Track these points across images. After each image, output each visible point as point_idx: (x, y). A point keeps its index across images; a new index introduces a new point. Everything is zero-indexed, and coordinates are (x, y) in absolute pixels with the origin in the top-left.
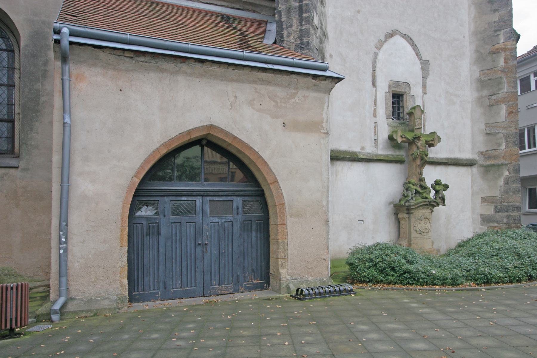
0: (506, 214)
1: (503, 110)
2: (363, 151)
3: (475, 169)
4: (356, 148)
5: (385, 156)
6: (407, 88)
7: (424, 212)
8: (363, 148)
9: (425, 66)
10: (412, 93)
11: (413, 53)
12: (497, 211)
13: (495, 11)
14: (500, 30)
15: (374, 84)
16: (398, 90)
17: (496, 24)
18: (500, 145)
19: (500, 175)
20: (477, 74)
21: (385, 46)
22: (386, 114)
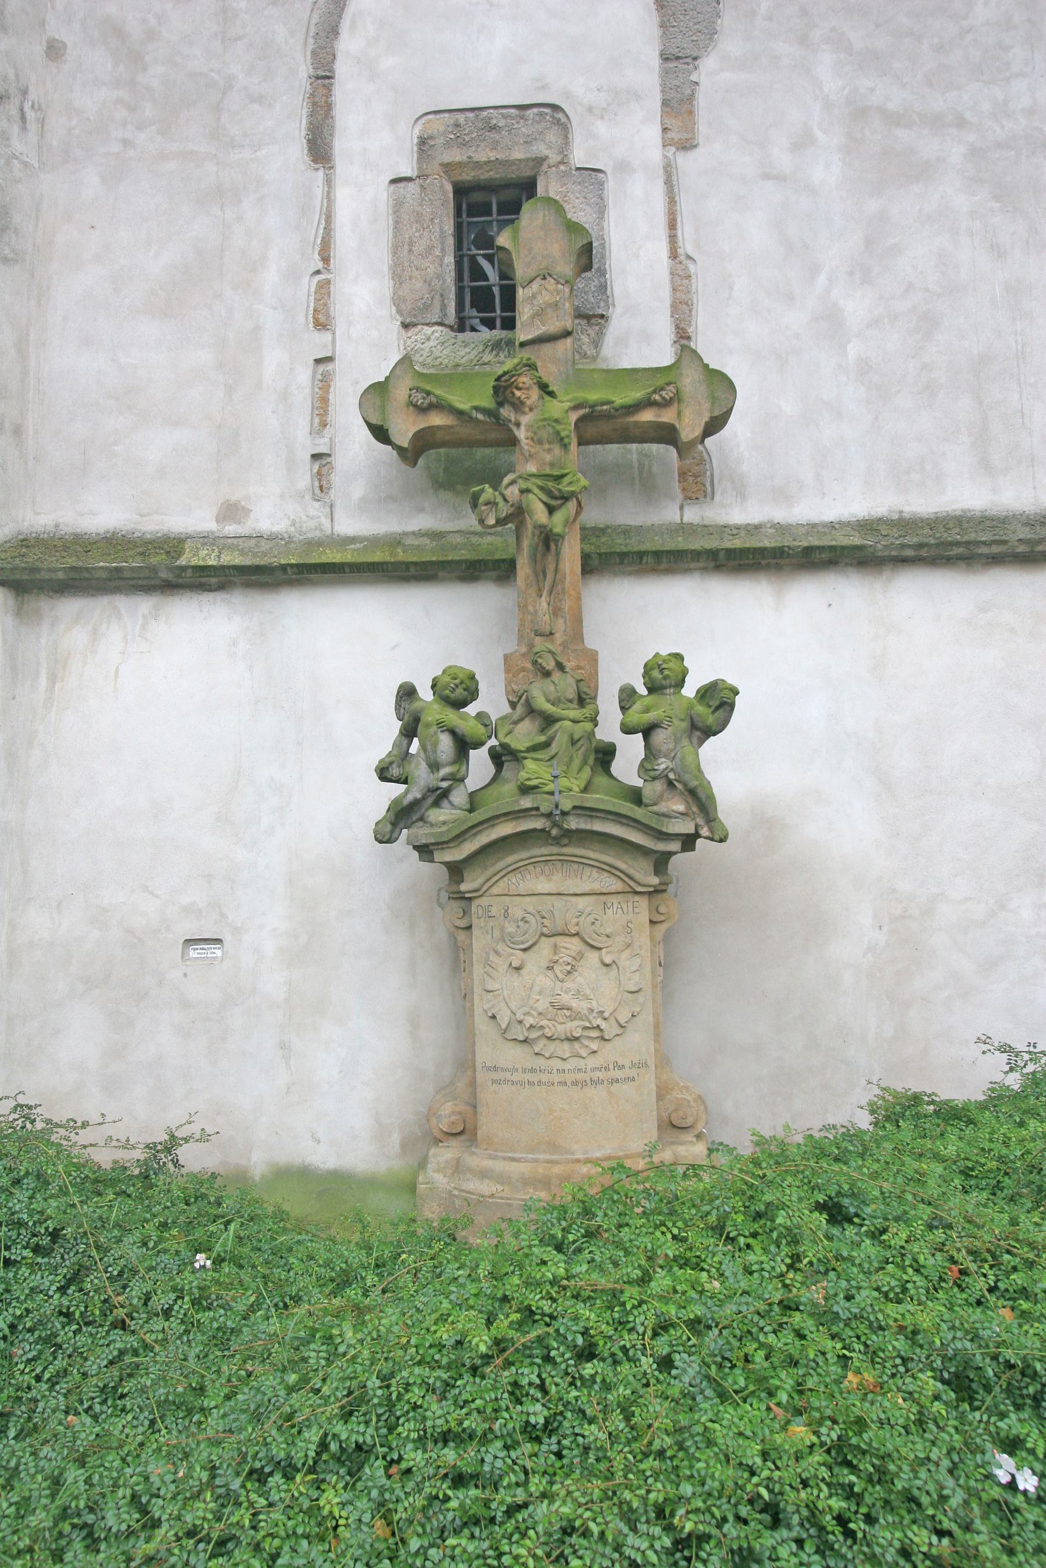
2: (231, 529)
4: (186, 514)
5: (374, 542)
6: (553, 136)
7: (543, 885)
8: (231, 511)
10: (579, 157)
15: (319, 150)
16: (483, 155)
22: (398, 301)
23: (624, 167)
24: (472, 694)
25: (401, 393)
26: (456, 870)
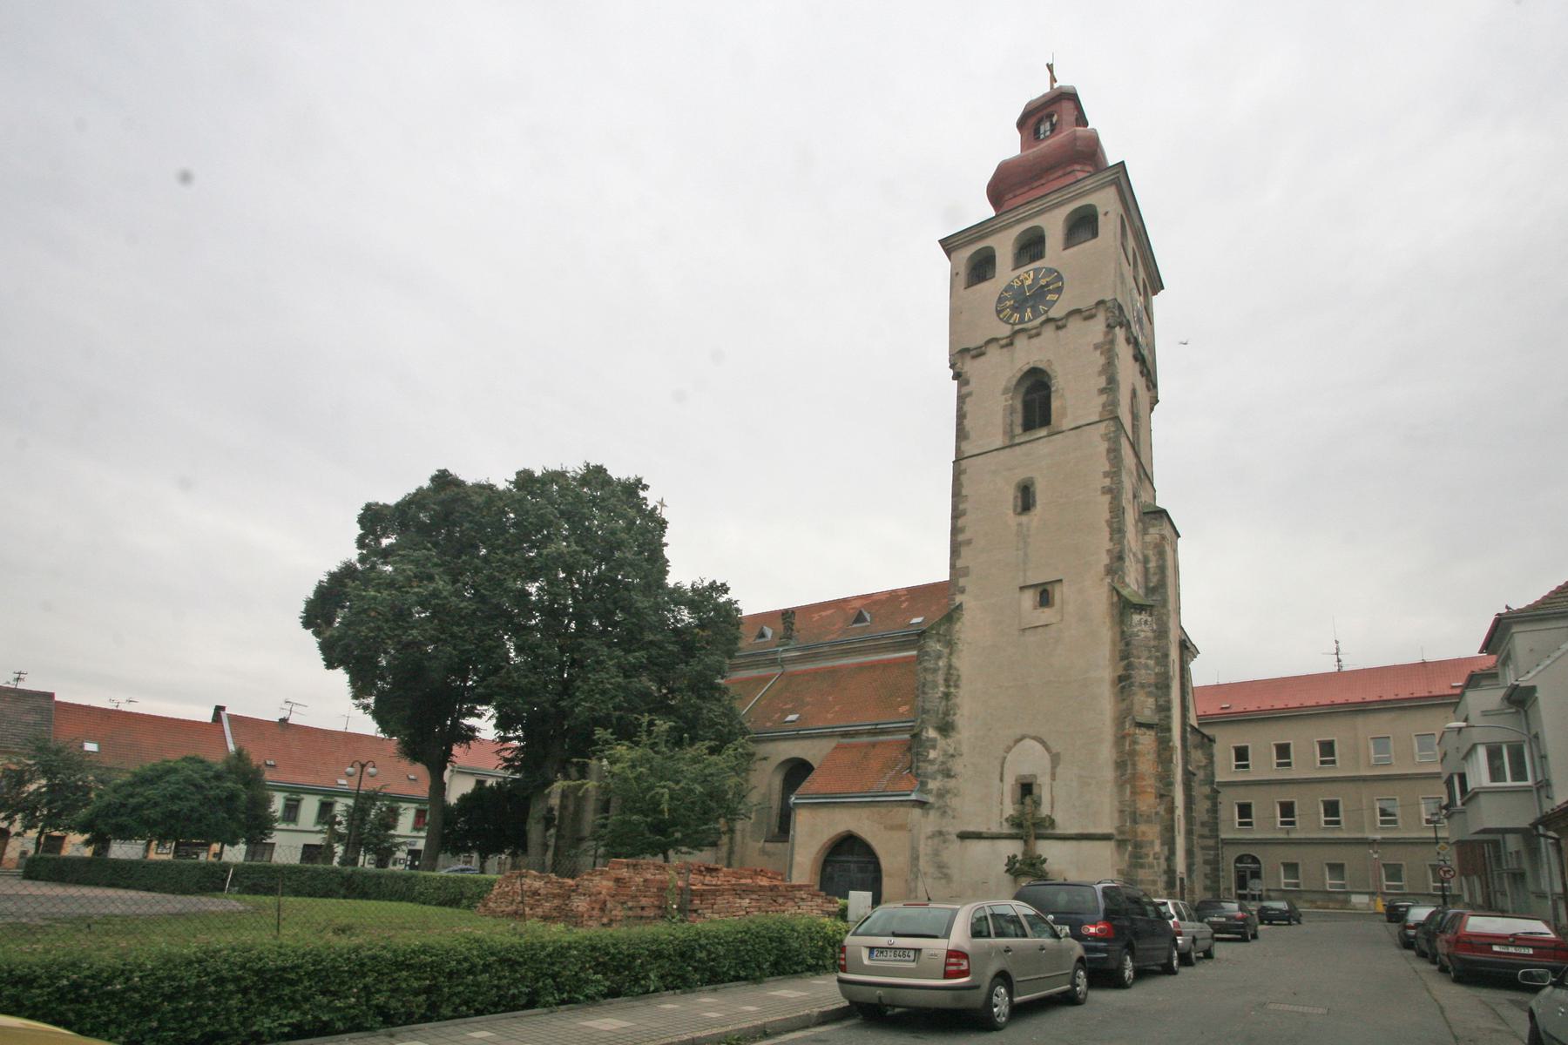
9: (1055, 759)
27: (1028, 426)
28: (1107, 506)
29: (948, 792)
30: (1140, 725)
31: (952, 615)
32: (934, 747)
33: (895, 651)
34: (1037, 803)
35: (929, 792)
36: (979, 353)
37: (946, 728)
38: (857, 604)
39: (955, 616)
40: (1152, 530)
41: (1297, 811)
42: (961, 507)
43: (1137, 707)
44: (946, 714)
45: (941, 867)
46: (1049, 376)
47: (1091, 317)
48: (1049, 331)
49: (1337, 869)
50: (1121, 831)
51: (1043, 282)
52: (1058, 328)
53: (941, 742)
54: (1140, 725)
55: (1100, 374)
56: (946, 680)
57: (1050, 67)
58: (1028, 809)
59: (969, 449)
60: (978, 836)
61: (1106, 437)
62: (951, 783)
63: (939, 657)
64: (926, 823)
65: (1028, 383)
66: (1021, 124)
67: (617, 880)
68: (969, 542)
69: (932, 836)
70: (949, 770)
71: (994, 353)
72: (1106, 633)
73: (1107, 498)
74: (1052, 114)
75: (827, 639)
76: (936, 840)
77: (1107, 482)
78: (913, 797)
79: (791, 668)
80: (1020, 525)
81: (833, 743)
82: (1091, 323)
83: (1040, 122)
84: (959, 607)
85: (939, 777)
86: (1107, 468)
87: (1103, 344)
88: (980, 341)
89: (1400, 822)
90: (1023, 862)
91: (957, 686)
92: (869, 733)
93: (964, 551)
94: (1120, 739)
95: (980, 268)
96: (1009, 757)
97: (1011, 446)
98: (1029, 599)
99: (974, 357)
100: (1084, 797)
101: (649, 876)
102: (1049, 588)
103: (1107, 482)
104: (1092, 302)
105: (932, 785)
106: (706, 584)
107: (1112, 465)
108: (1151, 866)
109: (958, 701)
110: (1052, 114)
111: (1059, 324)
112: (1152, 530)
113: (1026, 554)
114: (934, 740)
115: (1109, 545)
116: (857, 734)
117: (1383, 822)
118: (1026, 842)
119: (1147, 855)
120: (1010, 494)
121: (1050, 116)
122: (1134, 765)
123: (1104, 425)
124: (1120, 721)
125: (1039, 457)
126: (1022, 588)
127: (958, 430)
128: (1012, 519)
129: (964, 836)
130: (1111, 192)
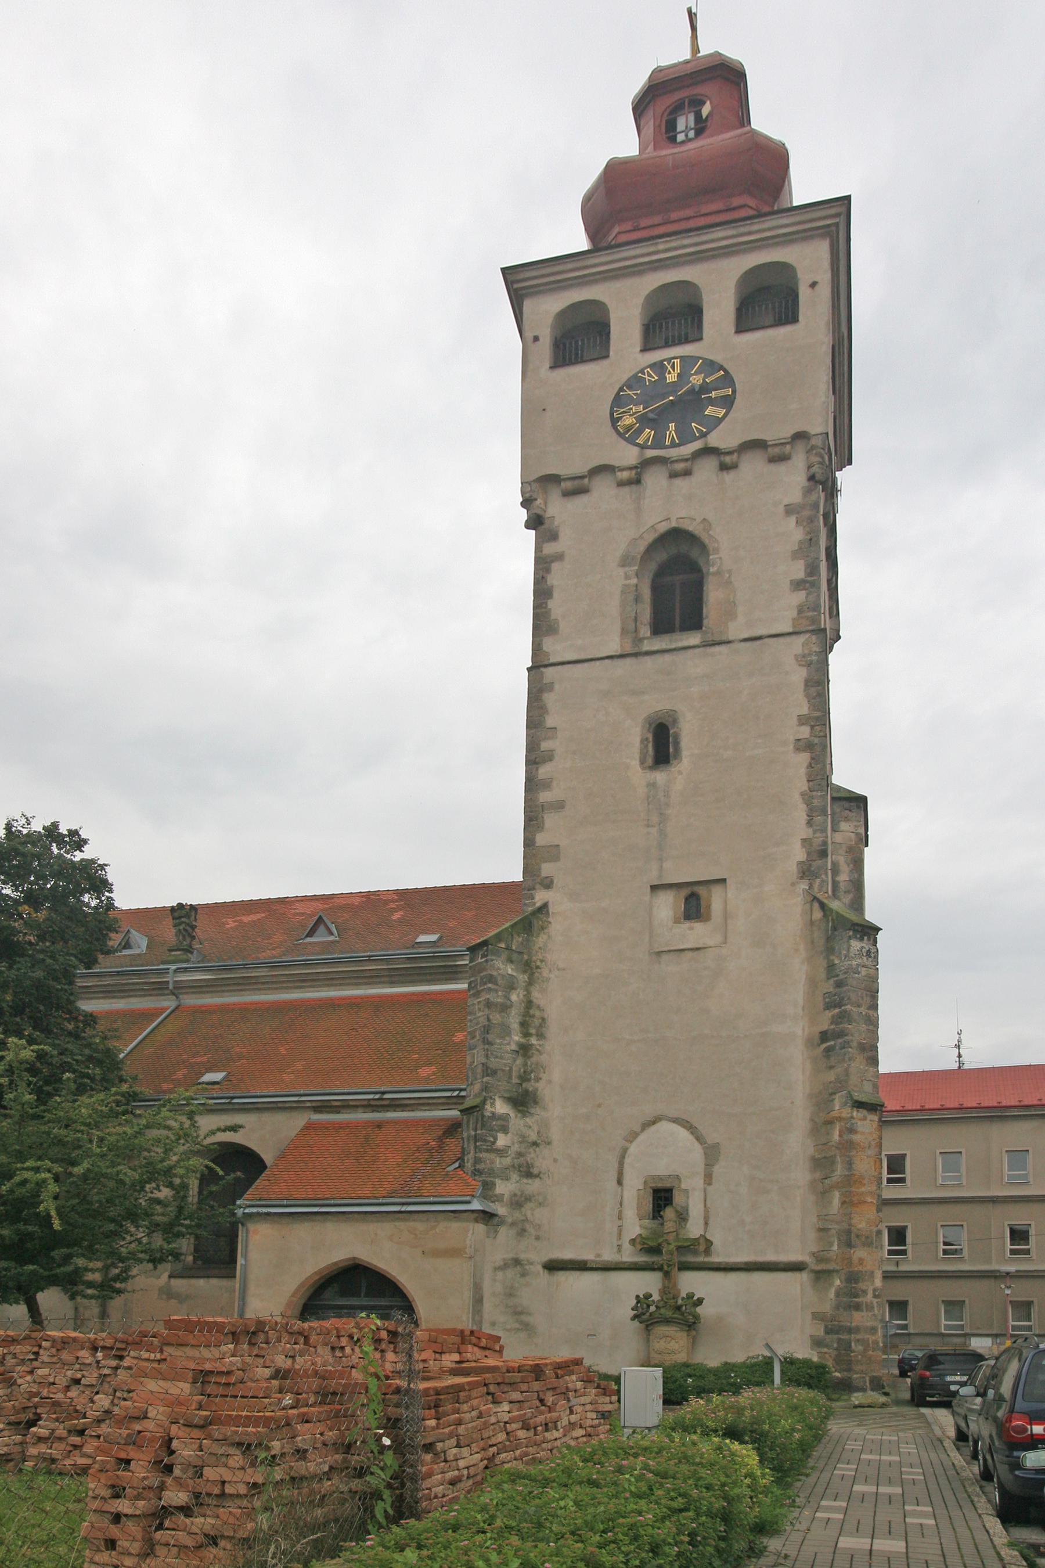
0: (835, 1336)
1: (836, 1198)
3: (804, 1276)
9: (712, 1154)
10: (683, 1186)
11: (691, 1137)
12: (828, 1331)
13: (831, 1067)
14: (835, 1094)
15: (620, 1182)
17: (832, 1085)
18: (831, 1244)
19: (831, 1285)
20: (811, 1151)
21: (641, 1137)
23: (694, 1189)
24: (651, 1296)
25: (638, 1241)
26: (647, 1326)
27: (661, 626)
28: (803, 771)
29: (529, 1199)
30: (859, 1105)
31: (532, 922)
32: (505, 1130)
33: (392, 984)
34: (682, 1217)
35: (499, 1198)
36: (577, 488)
37: (523, 1101)
38: (309, 908)
39: (537, 924)
40: (844, 826)
41: (909, 1239)
42: (545, 745)
43: (854, 1080)
44: (524, 1078)
45: (518, 1312)
46: (703, 548)
47: (783, 458)
48: (707, 468)
49: (954, 1306)
50: (819, 1258)
51: (696, 380)
52: (724, 467)
53: (516, 1122)
54: (859, 1105)
55: (795, 555)
56: (524, 1024)
57: (692, 16)
58: (669, 1226)
59: (557, 649)
60: (581, 1266)
61: (803, 660)
62: (532, 1186)
63: (511, 987)
64: (502, 1245)
65: (662, 556)
66: (640, 108)
67: (202, 1377)
68: (559, 806)
69: (505, 1266)
70: (529, 1166)
71: (603, 490)
72: (799, 969)
73: (804, 758)
74: (695, 95)
75: (264, 956)
76: (510, 1273)
77: (805, 732)
78: (476, 1205)
79: (191, 1000)
80: (652, 785)
81: (300, 1120)
82: (782, 468)
83: (677, 109)
84: (544, 908)
85: (515, 1177)
86: (805, 710)
87: (803, 507)
88: (580, 467)
89: (965, 1253)
90: (664, 1303)
91: (541, 1036)
92: (369, 1106)
93: (550, 820)
94: (821, 1125)
95: (577, 339)
96: (633, 1149)
97: (635, 655)
98: (666, 906)
99: (567, 494)
100: (760, 1205)
101: (281, 1361)
102: (701, 891)
103: (805, 732)
104: (788, 432)
105: (502, 1188)
106: (37, 826)
107: (813, 707)
108: (870, 1307)
109: (544, 1058)
110: (695, 95)
111: (726, 461)
112: (844, 826)
113: (662, 833)
114: (505, 1118)
115: (805, 832)
116: (346, 1106)
117: (1013, 1252)
118: (667, 1274)
119: (865, 1292)
120: (635, 737)
121: (697, 103)
122: (850, 1164)
123: (801, 639)
124: (821, 1100)
125: (685, 678)
126: (654, 888)
127: (536, 617)
128: (638, 776)
129: (553, 1266)
130: (822, 249)
